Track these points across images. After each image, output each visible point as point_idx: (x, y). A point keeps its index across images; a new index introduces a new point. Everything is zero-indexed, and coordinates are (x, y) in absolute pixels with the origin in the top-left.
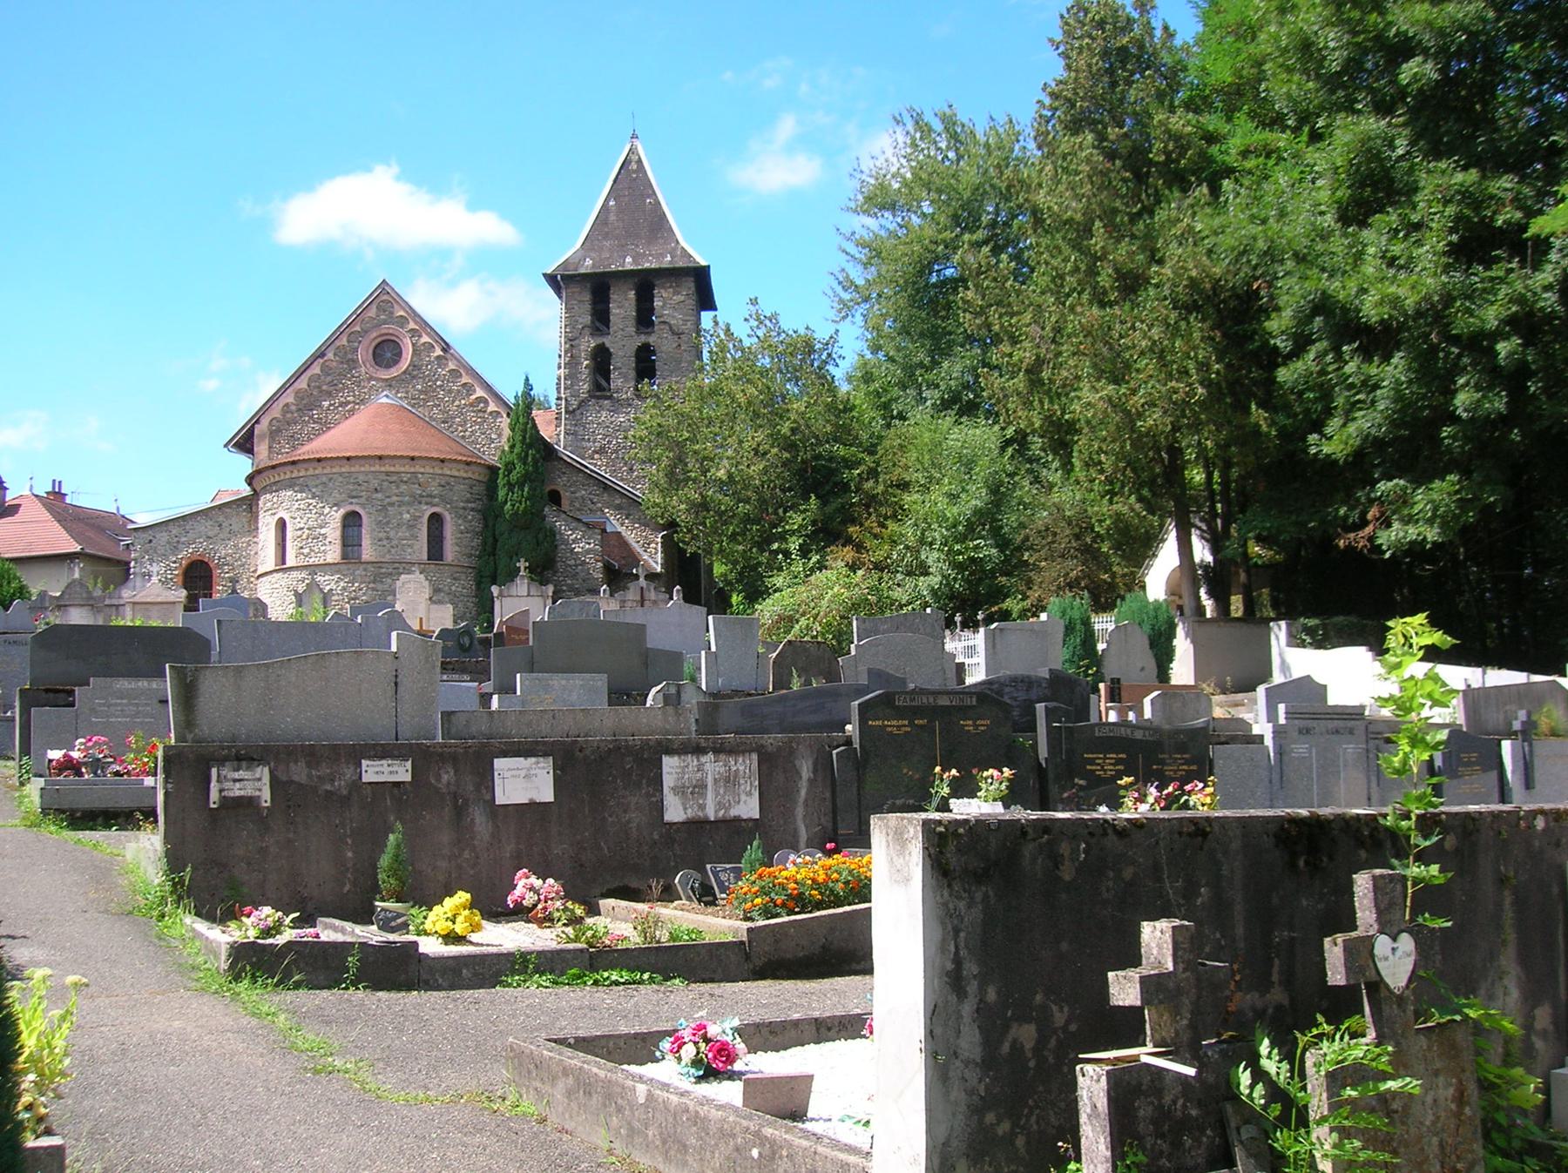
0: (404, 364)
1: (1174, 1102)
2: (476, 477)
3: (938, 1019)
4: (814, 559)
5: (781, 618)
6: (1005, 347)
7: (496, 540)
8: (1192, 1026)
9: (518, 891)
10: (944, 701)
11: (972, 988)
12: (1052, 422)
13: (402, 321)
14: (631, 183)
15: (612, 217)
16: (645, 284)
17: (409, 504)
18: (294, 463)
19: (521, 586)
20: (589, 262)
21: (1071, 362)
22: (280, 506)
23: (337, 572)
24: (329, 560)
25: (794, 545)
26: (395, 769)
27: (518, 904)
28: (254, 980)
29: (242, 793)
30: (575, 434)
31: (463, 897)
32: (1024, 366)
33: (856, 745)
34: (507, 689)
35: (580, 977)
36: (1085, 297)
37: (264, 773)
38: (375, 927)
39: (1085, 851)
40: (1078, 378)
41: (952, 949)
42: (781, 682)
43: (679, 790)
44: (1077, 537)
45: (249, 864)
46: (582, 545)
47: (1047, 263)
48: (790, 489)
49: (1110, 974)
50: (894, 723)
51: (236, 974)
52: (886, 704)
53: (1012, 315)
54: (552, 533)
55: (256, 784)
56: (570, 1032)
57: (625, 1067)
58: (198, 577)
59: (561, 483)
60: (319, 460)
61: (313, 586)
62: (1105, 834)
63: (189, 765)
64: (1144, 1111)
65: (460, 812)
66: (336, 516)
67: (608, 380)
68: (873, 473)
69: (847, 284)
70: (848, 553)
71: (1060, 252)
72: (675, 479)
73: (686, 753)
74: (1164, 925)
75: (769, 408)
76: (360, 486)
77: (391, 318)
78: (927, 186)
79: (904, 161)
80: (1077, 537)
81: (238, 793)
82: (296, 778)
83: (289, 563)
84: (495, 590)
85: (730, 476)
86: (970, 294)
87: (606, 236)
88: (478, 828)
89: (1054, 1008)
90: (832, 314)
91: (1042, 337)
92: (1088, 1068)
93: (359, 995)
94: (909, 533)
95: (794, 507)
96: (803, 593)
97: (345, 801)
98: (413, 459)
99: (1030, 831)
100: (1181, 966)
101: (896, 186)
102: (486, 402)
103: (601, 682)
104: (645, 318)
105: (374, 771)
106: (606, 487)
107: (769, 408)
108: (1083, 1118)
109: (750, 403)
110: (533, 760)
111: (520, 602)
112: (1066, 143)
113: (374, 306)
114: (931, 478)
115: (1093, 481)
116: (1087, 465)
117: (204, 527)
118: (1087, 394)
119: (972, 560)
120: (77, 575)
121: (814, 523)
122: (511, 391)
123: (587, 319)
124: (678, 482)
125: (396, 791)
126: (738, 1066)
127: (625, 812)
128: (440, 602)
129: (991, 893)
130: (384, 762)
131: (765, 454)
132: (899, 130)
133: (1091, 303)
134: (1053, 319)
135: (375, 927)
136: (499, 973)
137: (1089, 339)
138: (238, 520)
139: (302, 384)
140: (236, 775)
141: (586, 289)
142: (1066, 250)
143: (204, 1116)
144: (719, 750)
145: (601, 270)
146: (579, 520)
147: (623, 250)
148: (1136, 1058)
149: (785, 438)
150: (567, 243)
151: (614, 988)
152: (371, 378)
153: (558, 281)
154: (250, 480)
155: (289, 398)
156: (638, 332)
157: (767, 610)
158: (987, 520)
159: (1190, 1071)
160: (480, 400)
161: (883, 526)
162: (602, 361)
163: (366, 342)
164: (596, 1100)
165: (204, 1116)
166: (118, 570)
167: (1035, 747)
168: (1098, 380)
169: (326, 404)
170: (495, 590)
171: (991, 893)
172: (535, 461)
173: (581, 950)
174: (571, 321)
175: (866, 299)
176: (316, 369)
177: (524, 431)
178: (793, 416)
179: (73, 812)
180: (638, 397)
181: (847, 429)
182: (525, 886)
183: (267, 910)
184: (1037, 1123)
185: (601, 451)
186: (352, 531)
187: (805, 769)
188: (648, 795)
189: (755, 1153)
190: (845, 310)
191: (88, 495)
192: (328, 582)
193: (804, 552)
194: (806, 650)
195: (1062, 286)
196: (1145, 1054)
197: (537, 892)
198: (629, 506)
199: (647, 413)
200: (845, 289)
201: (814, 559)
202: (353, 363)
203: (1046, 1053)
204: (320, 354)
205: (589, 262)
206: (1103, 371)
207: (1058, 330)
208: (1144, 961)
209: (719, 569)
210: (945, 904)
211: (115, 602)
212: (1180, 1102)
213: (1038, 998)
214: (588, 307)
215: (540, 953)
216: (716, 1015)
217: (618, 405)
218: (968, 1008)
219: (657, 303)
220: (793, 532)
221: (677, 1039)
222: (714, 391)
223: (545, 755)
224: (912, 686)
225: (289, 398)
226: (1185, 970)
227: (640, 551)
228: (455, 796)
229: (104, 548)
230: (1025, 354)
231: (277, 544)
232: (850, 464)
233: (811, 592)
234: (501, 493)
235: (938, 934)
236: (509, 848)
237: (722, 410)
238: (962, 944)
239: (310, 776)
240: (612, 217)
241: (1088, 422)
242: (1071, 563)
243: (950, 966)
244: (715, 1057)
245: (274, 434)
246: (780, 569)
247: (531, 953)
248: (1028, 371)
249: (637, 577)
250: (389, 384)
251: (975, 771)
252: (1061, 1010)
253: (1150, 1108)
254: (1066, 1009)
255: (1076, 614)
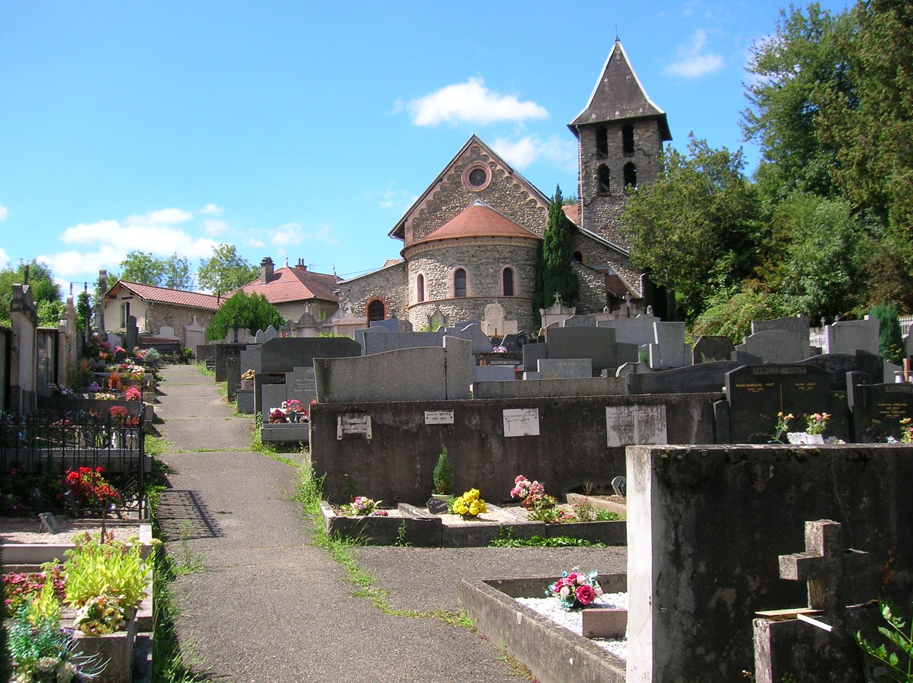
0: (487, 183)
1: (823, 648)
2: (531, 246)
3: (660, 581)
4: (735, 287)
5: (713, 324)
6: (843, 150)
7: (543, 282)
8: (838, 595)
9: (516, 489)
10: (785, 371)
11: (688, 563)
12: (875, 196)
13: (485, 158)
14: (617, 68)
15: (607, 89)
16: (628, 126)
17: (492, 263)
18: (426, 243)
19: (557, 308)
20: (594, 116)
21: (885, 157)
22: (421, 268)
23: (453, 304)
24: (448, 297)
25: (721, 279)
26: (444, 416)
27: (516, 496)
28: (344, 539)
29: (355, 431)
30: (589, 218)
31: (475, 492)
32: (855, 161)
33: (729, 400)
34: (532, 368)
35: (539, 541)
36: (893, 114)
37: (368, 419)
38: (427, 510)
39: (773, 471)
40: (890, 167)
41: (673, 537)
42: (698, 359)
43: (617, 428)
44: (898, 267)
45: (360, 472)
46: (594, 284)
47: (868, 96)
48: (718, 245)
49: (780, 557)
50: (753, 385)
51: (333, 535)
52: (747, 374)
53: (847, 129)
54: (576, 277)
55: (363, 426)
56: (498, 577)
57: (521, 600)
58: (376, 310)
59: (581, 247)
60: (440, 240)
61: (438, 312)
62: (789, 460)
63: (326, 415)
64: (799, 653)
65: (483, 441)
66: (451, 272)
67: (608, 185)
68: (768, 234)
69: (751, 118)
70: (755, 283)
71: (876, 88)
72: (648, 241)
73: (620, 405)
74: (819, 524)
75: (703, 196)
76: (463, 254)
77: (479, 157)
78: (798, 54)
79: (783, 40)
80: (898, 267)
81: (353, 431)
82: (386, 422)
83: (426, 300)
84: (542, 311)
85: (681, 239)
86: (820, 119)
87: (603, 100)
88: (494, 451)
89: (750, 578)
90: (742, 137)
91: (866, 143)
92: (760, 621)
93: (404, 550)
94: (792, 268)
95: (720, 256)
96: (726, 308)
97: (415, 435)
98: (493, 237)
99: (731, 457)
100: (830, 554)
101: (778, 56)
102: (535, 202)
103: (587, 363)
104: (628, 147)
105: (432, 418)
106: (608, 249)
107: (703, 196)
108: (757, 656)
109: (691, 194)
110: (527, 410)
111: (556, 317)
112: (878, 18)
113: (469, 150)
114: (805, 235)
115: (901, 231)
116: (898, 221)
117: (379, 281)
118: (895, 177)
119: (833, 284)
120: (307, 311)
121: (733, 266)
122: (550, 193)
123: (594, 150)
124: (651, 244)
125: (445, 429)
126: (597, 601)
127: (584, 441)
128: (510, 319)
129: (702, 499)
130: (437, 412)
131: (701, 225)
132: (782, 18)
133: (896, 118)
134: (873, 131)
135: (427, 510)
136: (490, 538)
137: (896, 142)
138: (397, 277)
139: (430, 197)
140: (352, 421)
141: (593, 132)
142: (880, 86)
143: (279, 619)
144: (641, 403)
145: (601, 120)
146: (592, 269)
147: (613, 108)
148: (794, 616)
149: (713, 214)
150: (581, 106)
151: (559, 548)
152: (469, 192)
153: (577, 129)
154: (403, 253)
155: (423, 206)
156: (625, 156)
157: (704, 319)
158: (843, 257)
159: (828, 628)
160: (532, 201)
161: (775, 265)
162: (604, 174)
163: (465, 171)
164: (499, 620)
165: (279, 619)
166: (331, 306)
167: (845, 399)
168: (903, 166)
169: (444, 208)
170: (542, 311)
171: (702, 499)
172: (565, 235)
173: (541, 525)
174: (584, 152)
175: (763, 126)
176: (438, 188)
177: (558, 218)
178: (717, 201)
179: (279, 442)
180: (626, 194)
181: (750, 208)
182: (521, 485)
183: (364, 499)
184: (736, 654)
185: (606, 227)
186: (460, 280)
187: (696, 414)
188: (598, 431)
189: (571, 661)
190: (749, 134)
191: (319, 266)
192: (447, 310)
193: (728, 283)
194: (714, 341)
195: (878, 109)
196: (802, 614)
197: (528, 489)
198: (622, 259)
199: (631, 204)
200: (750, 121)
201: (735, 287)
202: (458, 184)
203: (743, 608)
204: (439, 180)
205: (594, 116)
206: (906, 162)
207: (876, 137)
208: (807, 549)
209: (679, 296)
210: (668, 507)
211: (328, 325)
212: (828, 648)
213: (738, 571)
214: (594, 143)
215: (515, 527)
216: (585, 570)
217: (614, 200)
218: (684, 577)
219: (635, 138)
220: (720, 272)
221: (560, 583)
222: (670, 189)
223: (534, 407)
224: (766, 362)
225: (423, 206)
226: (833, 556)
227: (630, 285)
228: (480, 432)
229: (325, 294)
230: (856, 154)
231: (419, 289)
232: (754, 230)
233: (732, 308)
234: (545, 255)
235: (663, 526)
236: (513, 463)
237: (675, 200)
238: (681, 533)
239: (394, 421)
240: (607, 89)
241: (898, 194)
242: (894, 284)
243: (671, 548)
244: (581, 596)
245: (415, 227)
246: (713, 294)
247: (509, 526)
248: (859, 164)
249: (625, 301)
250: (479, 195)
251: (805, 415)
252: (755, 579)
253: (803, 652)
254: (758, 579)
255: (888, 315)
